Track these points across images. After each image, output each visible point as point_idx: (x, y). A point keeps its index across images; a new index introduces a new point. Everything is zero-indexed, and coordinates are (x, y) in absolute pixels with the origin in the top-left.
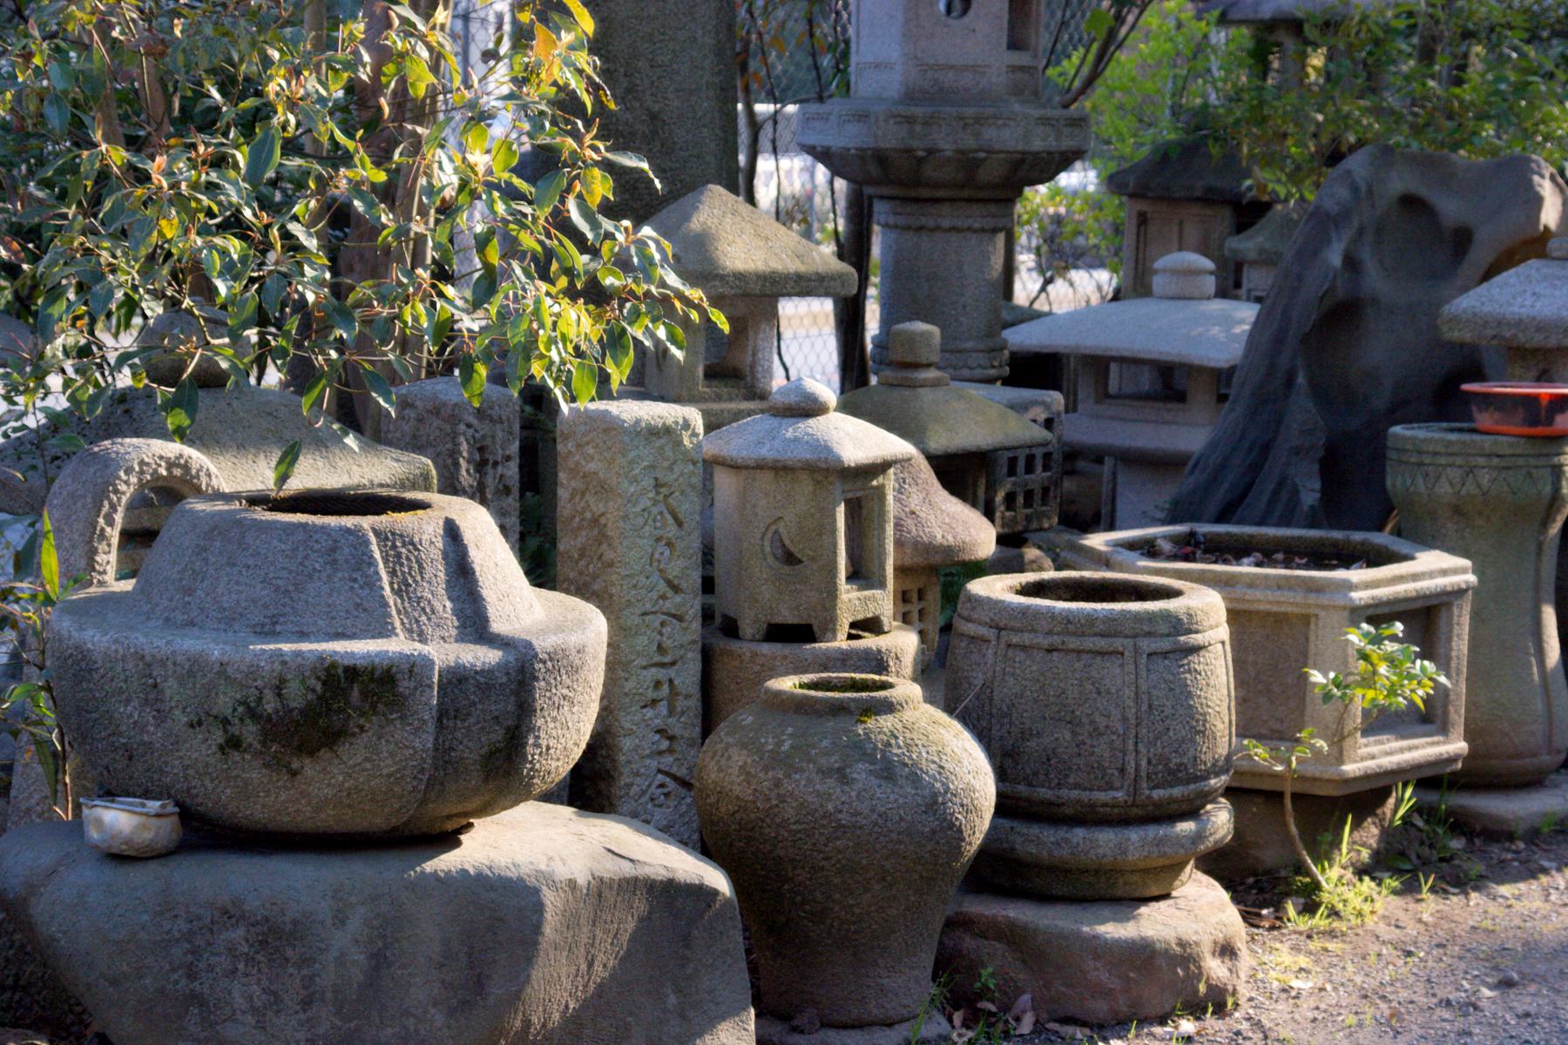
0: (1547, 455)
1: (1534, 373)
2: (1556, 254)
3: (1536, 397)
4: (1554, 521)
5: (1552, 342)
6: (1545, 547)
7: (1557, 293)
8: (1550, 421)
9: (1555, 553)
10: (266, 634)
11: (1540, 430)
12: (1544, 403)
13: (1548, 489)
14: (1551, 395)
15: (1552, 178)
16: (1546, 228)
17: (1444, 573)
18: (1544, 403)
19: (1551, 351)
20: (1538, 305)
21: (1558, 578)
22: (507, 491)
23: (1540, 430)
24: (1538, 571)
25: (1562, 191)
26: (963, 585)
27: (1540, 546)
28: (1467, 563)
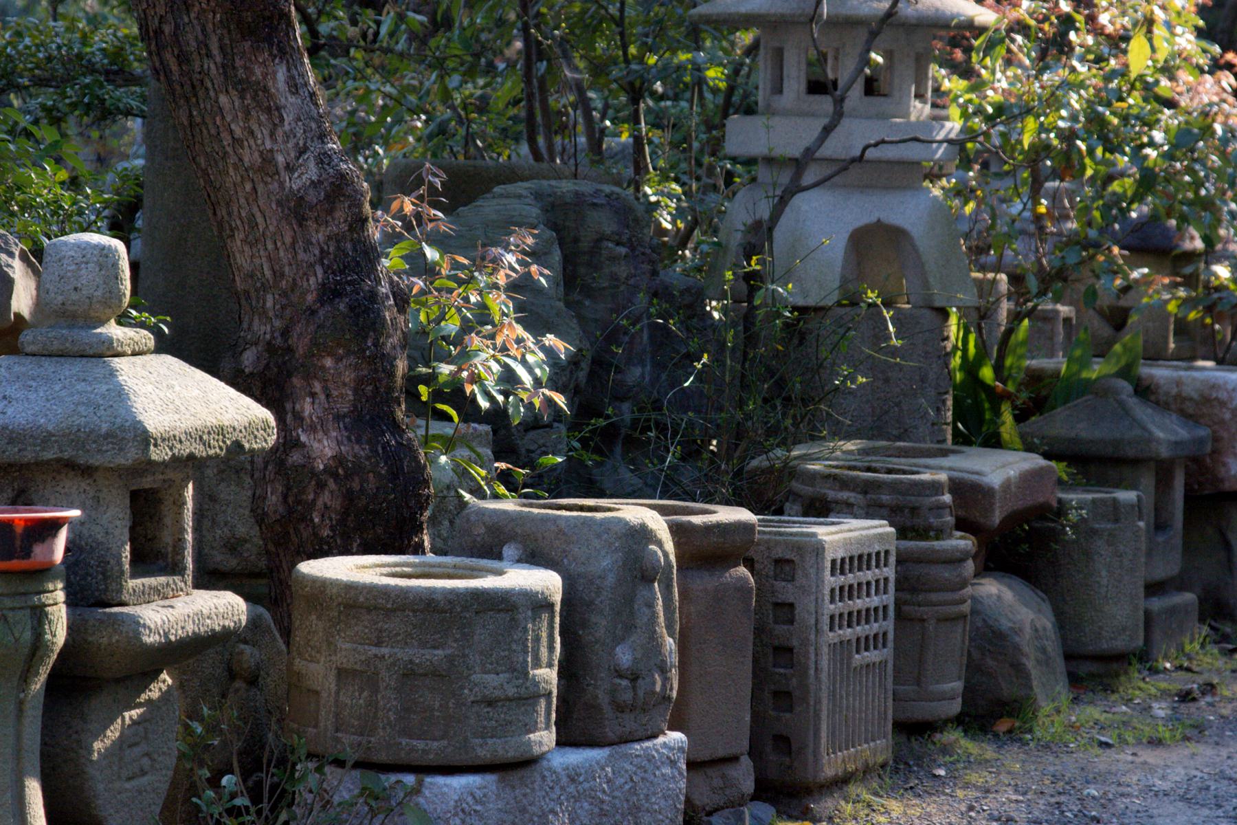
0: (24, 594)
1: (9, 493)
2: (29, 349)
3: (13, 520)
4: (37, 674)
5: (28, 456)
6: (27, 706)
7: (32, 396)
8: (27, 554)
9: (39, 712)
10: (867, 187)
11: (16, 564)
12: (19, 529)
13: (28, 635)
14: (27, 520)
15: (24, 257)
16: (18, 316)
17: (868, 528)
18: (19, 529)
19: (28, 465)
20: (10, 411)
21: (44, 744)
22: (124, 20)
23: (16, 564)
24: (18, 737)
25: (36, 272)
26: (294, 564)
27: (21, 703)
28: (885, 522)
